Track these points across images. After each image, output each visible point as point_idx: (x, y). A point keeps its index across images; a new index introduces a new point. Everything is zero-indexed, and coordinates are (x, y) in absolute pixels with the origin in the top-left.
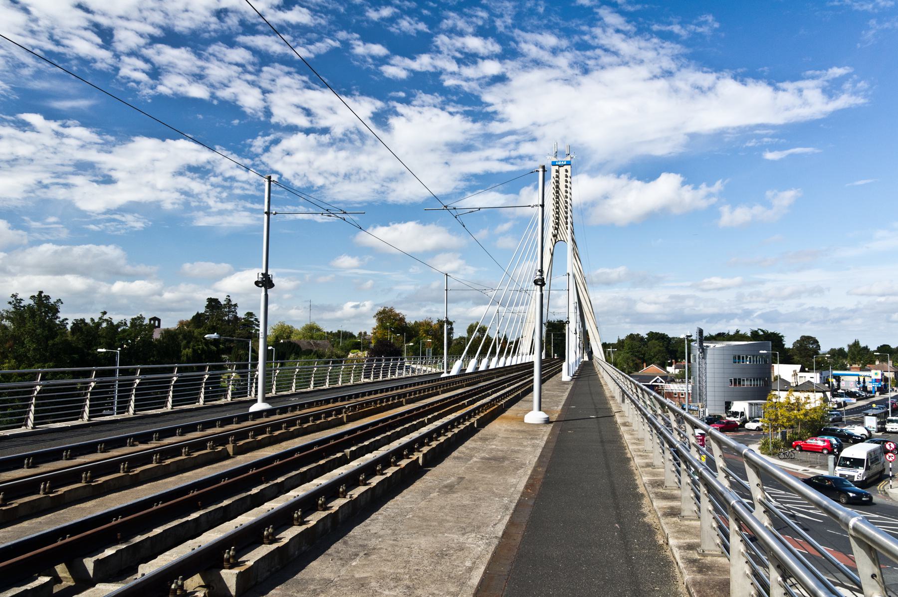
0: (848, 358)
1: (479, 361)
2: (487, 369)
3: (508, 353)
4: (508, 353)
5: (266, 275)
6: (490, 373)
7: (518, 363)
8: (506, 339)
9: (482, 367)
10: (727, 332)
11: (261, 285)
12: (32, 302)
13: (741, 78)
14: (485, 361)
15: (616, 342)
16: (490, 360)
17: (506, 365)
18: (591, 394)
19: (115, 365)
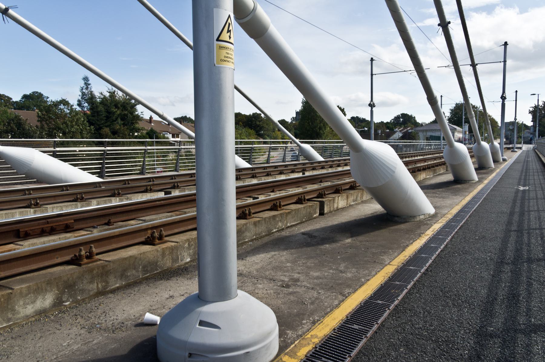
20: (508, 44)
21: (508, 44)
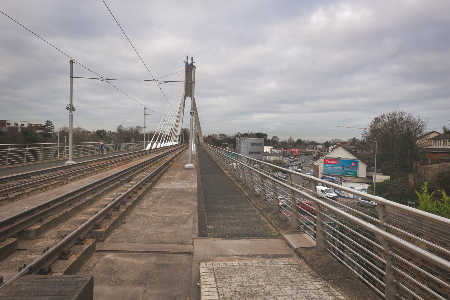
0: (401, 179)
1: (152, 144)
2: (156, 149)
3: (162, 140)
4: (159, 141)
5: (71, 104)
6: (165, 148)
7: (167, 146)
8: (161, 134)
9: (154, 147)
10: (260, 132)
11: (69, 109)
12: (129, 129)
13: (301, 140)
14: (159, 144)
15: (114, 130)
16: (157, 144)
17: (157, 147)
18: (244, 151)
19: (58, 143)
20: (196, 68)
21: (196, 68)
